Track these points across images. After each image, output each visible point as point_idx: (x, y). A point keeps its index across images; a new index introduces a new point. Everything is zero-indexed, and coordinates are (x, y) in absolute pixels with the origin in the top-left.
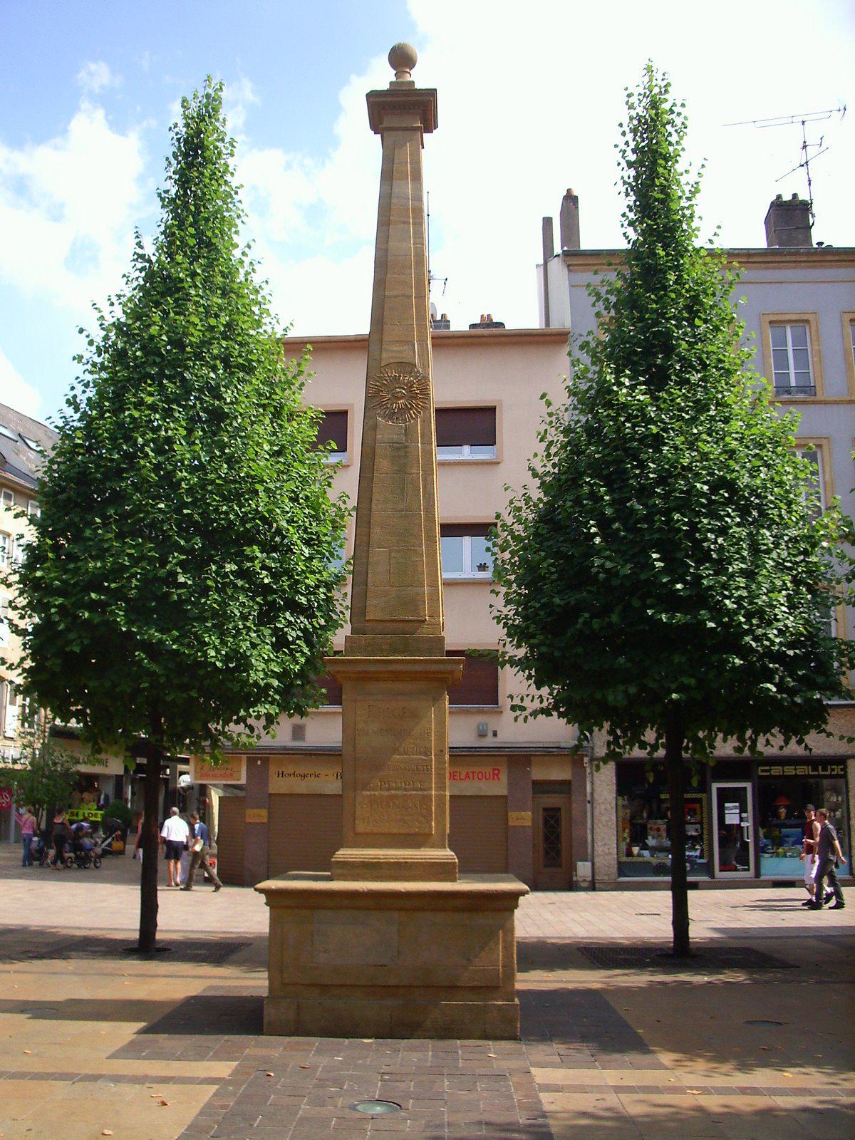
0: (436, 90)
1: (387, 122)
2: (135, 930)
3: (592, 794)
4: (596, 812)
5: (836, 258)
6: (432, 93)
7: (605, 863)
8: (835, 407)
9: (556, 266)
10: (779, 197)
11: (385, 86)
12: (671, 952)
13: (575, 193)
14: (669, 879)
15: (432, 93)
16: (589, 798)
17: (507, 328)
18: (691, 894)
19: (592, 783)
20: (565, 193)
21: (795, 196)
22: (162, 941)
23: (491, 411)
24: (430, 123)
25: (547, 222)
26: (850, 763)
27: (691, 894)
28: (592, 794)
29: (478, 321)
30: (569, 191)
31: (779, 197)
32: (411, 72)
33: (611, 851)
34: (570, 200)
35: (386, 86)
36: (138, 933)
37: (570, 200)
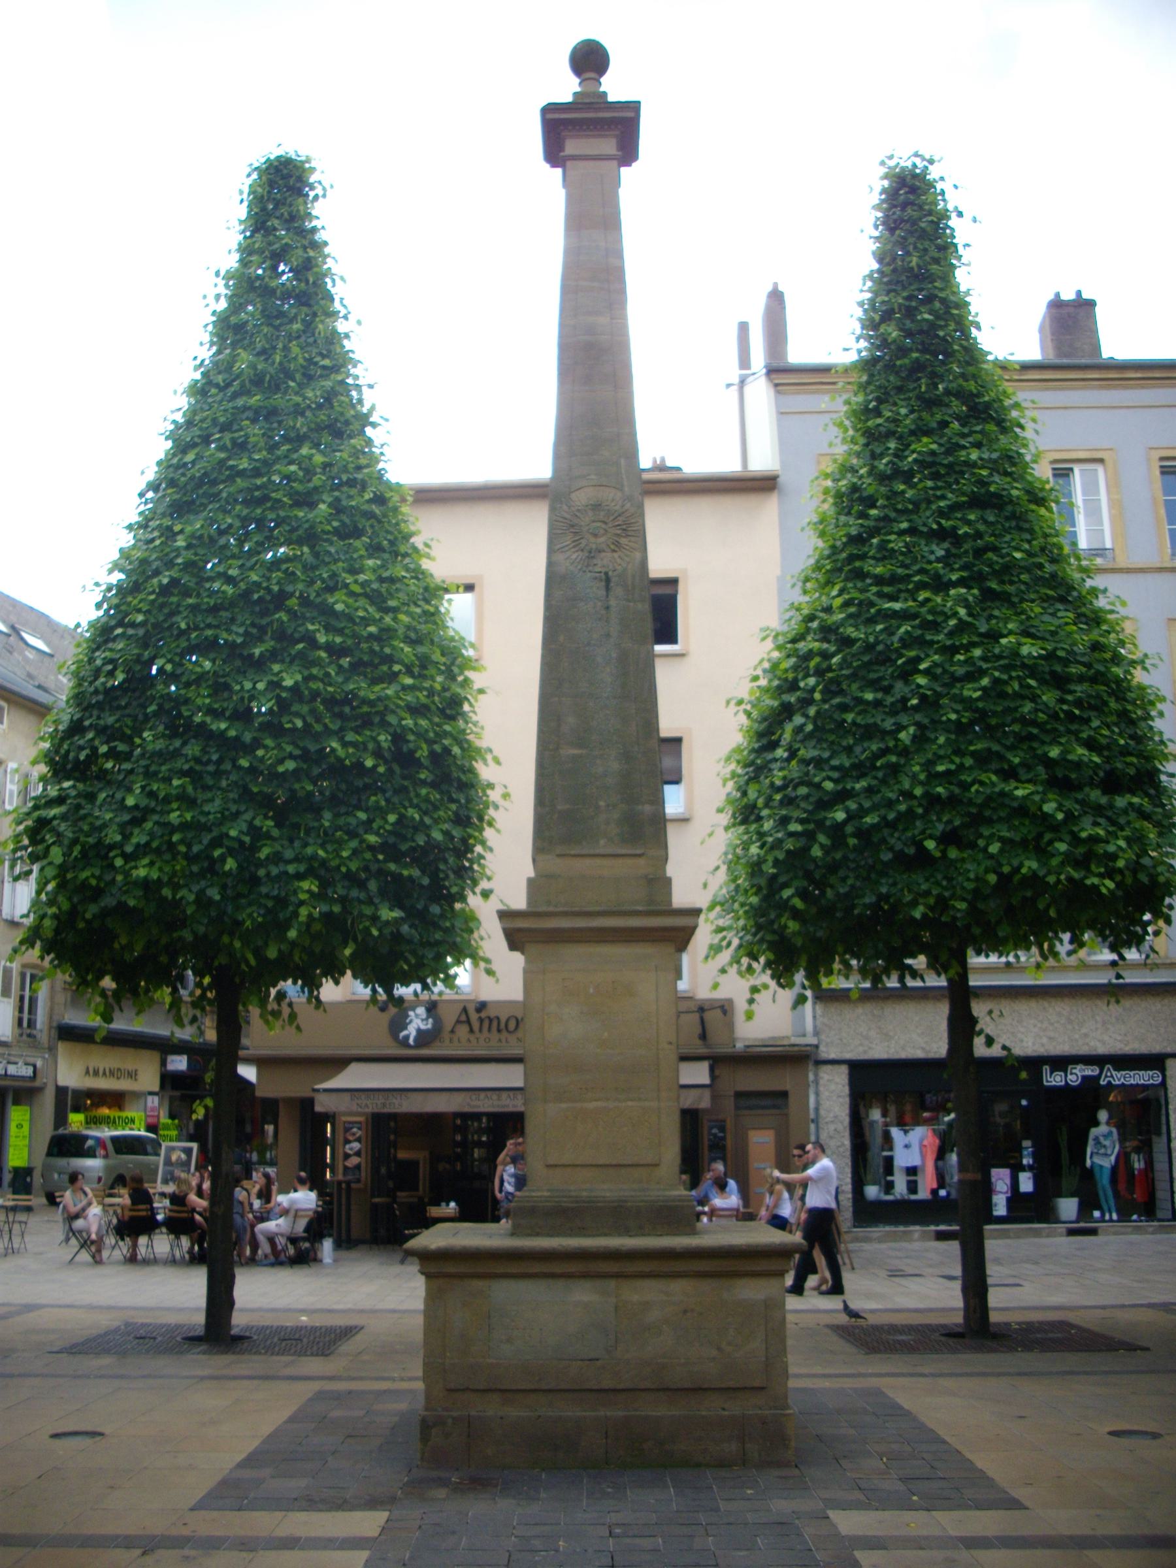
0: (639, 103)
1: (572, 146)
2: (197, 1309)
3: (817, 1109)
5: (1139, 375)
6: (633, 108)
8: (1140, 576)
10: (1057, 295)
12: (960, 1330)
13: (780, 288)
15: (633, 108)
16: (812, 1115)
19: (817, 1094)
21: (1079, 293)
22: (998, 1324)
23: (674, 582)
24: (628, 152)
25: (743, 328)
26: (1170, 1063)
28: (817, 1109)
30: (776, 285)
31: (1057, 295)
34: (776, 298)
35: (568, 98)
36: (961, 1313)
37: (776, 298)
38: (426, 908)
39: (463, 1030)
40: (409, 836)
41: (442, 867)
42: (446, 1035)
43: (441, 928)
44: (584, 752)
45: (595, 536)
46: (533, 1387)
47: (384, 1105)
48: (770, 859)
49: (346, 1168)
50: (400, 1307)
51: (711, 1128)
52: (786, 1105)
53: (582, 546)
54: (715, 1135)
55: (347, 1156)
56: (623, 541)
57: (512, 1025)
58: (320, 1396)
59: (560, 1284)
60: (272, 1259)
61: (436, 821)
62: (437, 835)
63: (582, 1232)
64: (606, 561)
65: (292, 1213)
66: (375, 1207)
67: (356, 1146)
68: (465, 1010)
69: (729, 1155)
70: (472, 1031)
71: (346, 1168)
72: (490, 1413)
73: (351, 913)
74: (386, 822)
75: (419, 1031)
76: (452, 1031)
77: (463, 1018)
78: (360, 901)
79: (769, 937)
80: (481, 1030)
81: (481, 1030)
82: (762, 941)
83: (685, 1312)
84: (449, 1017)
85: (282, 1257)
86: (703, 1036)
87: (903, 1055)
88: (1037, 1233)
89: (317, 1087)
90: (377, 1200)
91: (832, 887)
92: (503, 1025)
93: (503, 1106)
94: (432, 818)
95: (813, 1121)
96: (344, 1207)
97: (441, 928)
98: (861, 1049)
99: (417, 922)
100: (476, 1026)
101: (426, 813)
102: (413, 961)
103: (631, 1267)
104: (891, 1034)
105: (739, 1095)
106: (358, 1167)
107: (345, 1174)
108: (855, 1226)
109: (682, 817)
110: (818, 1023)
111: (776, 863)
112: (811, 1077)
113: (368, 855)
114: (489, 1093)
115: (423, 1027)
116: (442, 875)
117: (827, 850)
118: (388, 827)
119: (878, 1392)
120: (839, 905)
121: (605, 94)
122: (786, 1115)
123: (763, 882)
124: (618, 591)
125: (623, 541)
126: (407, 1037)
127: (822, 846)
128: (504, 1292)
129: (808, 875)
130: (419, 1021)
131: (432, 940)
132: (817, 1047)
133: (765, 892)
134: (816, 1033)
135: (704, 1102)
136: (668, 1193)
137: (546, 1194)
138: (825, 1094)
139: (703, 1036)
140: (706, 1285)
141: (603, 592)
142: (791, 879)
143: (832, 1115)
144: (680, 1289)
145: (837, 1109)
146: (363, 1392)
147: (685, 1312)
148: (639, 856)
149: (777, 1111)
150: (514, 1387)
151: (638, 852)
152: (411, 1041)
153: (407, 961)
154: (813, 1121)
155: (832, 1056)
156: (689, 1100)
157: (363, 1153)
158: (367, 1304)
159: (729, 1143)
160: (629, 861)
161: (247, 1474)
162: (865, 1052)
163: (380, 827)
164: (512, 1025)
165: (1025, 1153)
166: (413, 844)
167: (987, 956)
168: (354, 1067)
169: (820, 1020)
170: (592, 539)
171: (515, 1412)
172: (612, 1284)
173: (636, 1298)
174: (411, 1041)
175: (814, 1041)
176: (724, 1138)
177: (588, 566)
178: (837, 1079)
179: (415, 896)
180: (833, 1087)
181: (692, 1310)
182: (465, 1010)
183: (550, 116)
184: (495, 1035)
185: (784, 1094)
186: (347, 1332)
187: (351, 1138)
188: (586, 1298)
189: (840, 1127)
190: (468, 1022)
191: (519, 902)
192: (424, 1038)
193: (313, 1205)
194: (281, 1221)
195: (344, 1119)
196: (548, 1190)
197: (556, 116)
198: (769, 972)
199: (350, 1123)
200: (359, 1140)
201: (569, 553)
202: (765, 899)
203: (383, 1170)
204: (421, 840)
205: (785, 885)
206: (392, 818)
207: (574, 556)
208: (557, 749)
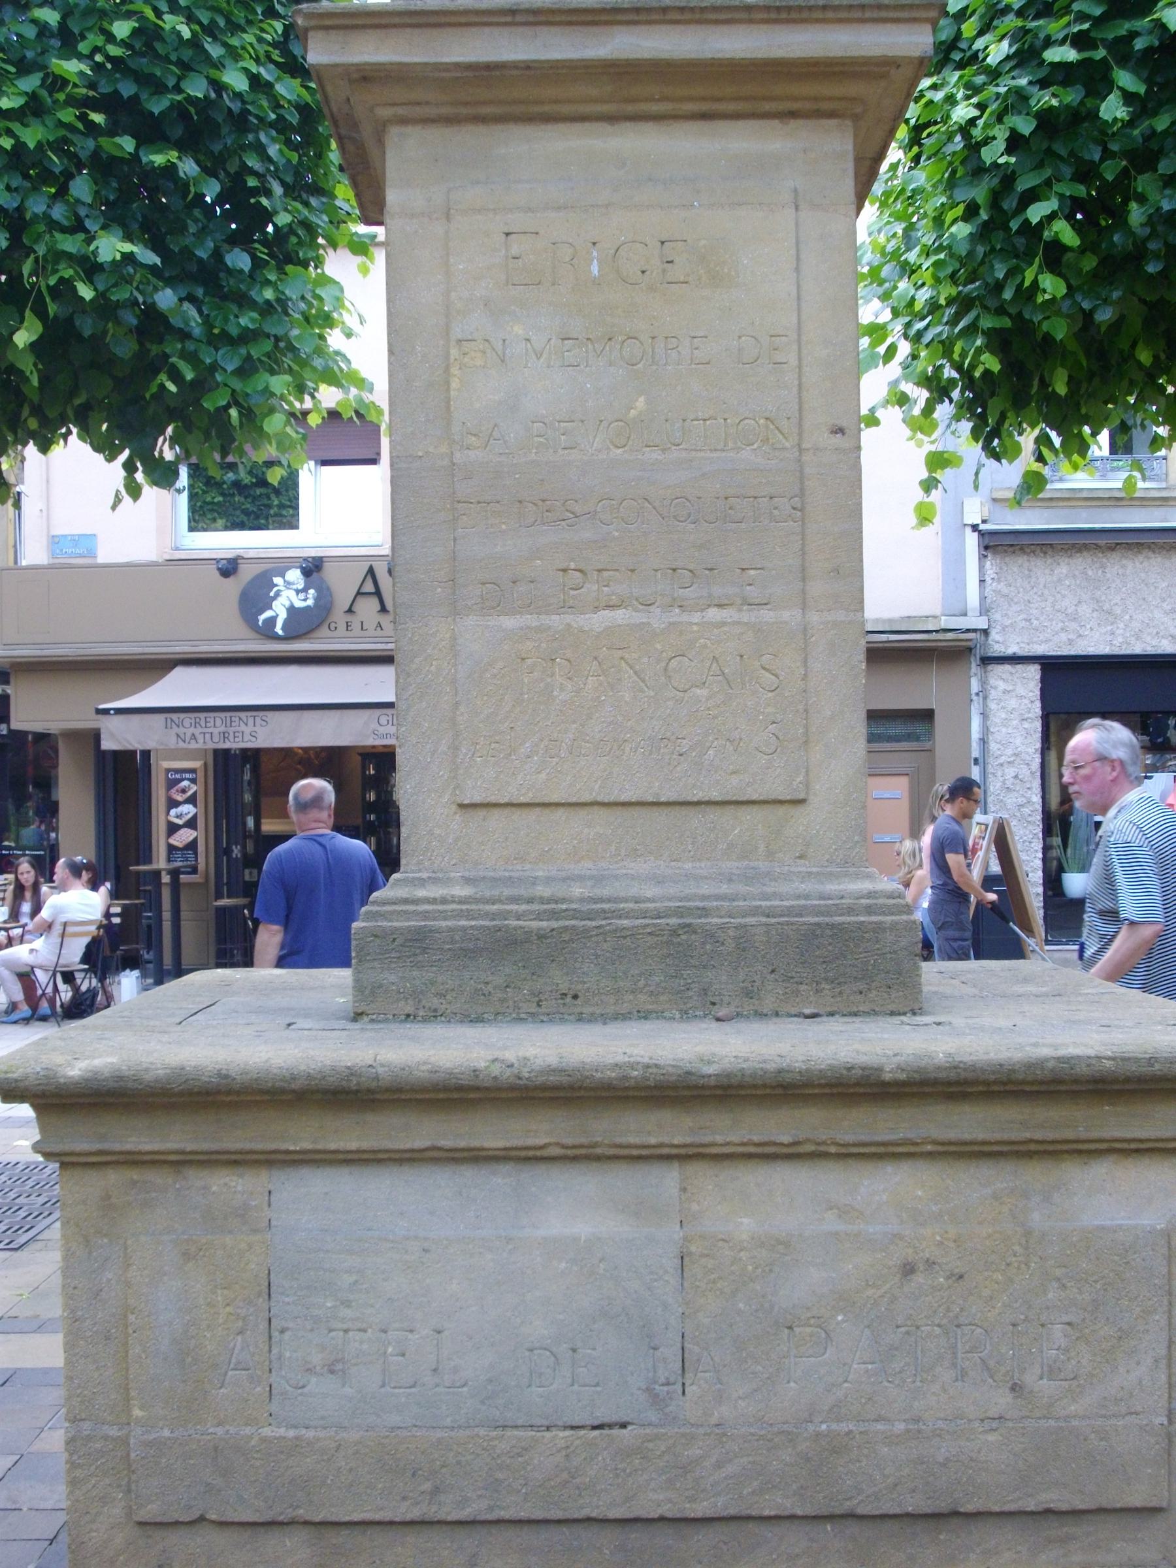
3: (984, 741)
19: (984, 715)
28: (984, 741)
38: (217, 255)
40: (171, 83)
41: (252, 162)
43: (252, 304)
46: (415, 1514)
47: (224, 736)
48: (1001, 134)
49: (171, 849)
52: (930, 734)
55: (173, 829)
59: (501, 1179)
60: (25, 1010)
61: (234, 54)
62: (236, 80)
65: (57, 929)
66: (221, 912)
67: (188, 810)
68: (371, 571)
71: (171, 849)
73: (30, 251)
74: (110, 38)
75: (292, 610)
76: (350, 611)
77: (369, 587)
78: (53, 225)
79: (988, 322)
82: (972, 330)
83: (908, 1270)
84: (344, 587)
85: (44, 1007)
87: (1137, 649)
90: (224, 902)
91: (1142, 199)
94: (225, 45)
97: (252, 304)
98: (1064, 637)
99: (200, 292)
101: (210, 30)
102: (189, 376)
104: (1118, 610)
106: (192, 846)
107: (169, 860)
110: (988, 591)
111: (1015, 142)
112: (975, 686)
113: (68, 115)
115: (299, 604)
116: (252, 182)
117: (1140, 105)
118: (114, 51)
120: (1152, 246)
123: (980, 193)
126: (272, 621)
127: (1129, 97)
129: (1085, 173)
130: (292, 594)
131: (234, 332)
132: (985, 632)
133: (984, 216)
134: (984, 610)
136: (832, 887)
137: (459, 891)
138: (997, 716)
142: (1048, 183)
143: (1009, 752)
145: (1018, 741)
147: (908, 1270)
149: (913, 745)
150: (356, 1517)
152: (279, 630)
153: (176, 376)
154: (976, 761)
155: (1012, 649)
157: (201, 823)
162: (1070, 642)
163: (96, 50)
166: (179, 98)
168: (179, 672)
169: (991, 586)
172: (669, 1179)
173: (746, 1226)
174: (279, 630)
178: (1021, 691)
179: (192, 229)
180: (1013, 703)
181: (930, 1264)
182: (371, 571)
185: (927, 716)
187: (180, 798)
188: (583, 1228)
189: (1024, 772)
190: (378, 593)
193: (97, 914)
194: (39, 943)
195: (166, 764)
196: (468, 881)
198: (966, 426)
199: (177, 771)
200: (192, 800)
202: (983, 233)
203: (236, 851)
204: (197, 88)
205: (1031, 197)
206: (122, 29)
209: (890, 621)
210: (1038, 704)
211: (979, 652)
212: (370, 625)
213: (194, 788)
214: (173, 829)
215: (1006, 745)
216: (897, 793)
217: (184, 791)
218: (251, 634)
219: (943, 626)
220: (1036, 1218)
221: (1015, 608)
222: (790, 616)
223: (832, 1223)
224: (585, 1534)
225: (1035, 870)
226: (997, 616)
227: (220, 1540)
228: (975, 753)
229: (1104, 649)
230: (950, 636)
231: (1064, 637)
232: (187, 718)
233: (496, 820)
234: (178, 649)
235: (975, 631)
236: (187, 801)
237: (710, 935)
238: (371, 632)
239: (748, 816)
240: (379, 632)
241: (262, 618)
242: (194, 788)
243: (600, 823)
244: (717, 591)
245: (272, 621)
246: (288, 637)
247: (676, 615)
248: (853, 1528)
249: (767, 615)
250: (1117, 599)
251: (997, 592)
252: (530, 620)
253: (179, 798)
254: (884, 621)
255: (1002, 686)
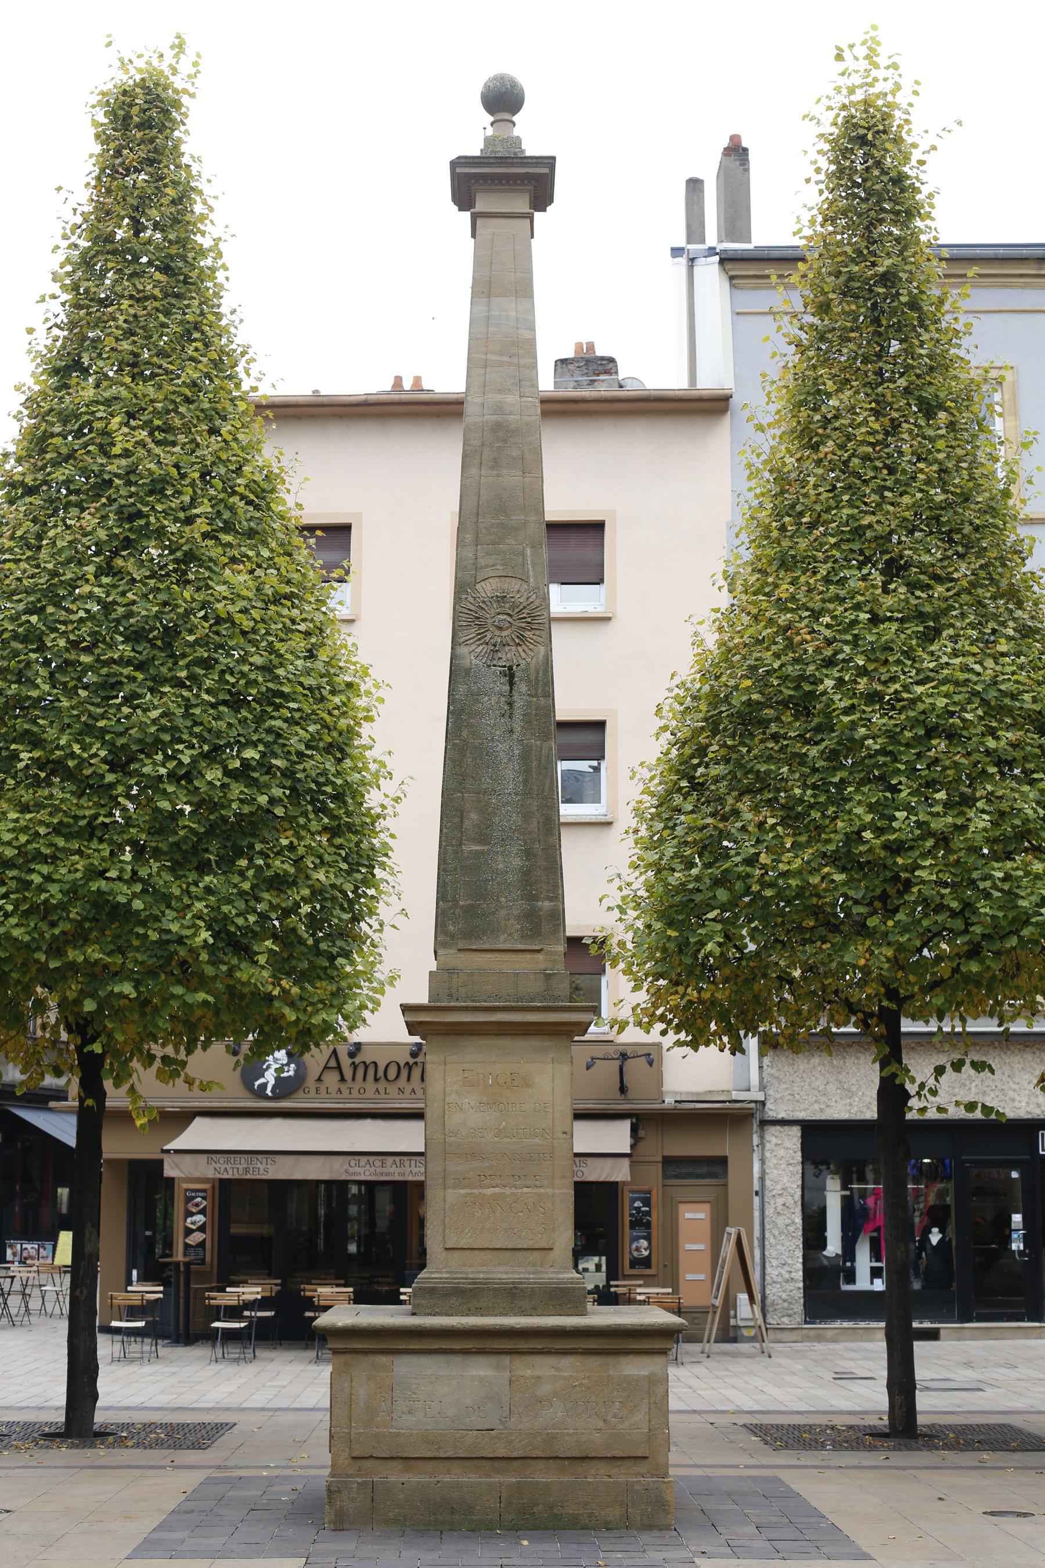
0: (554, 158)
2: (57, 1409)
3: (762, 1179)
4: (769, 1211)
6: (550, 162)
7: (784, 1296)
9: (709, 272)
11: (474, 149)
14: (883, 1325)
15: (550, 162)
17: (623, 373)
18: (920, 1348)
19: (763, 1161)
20: (726, 143)
25: (694, 186)
27: (920, 1348)
28: (762, 1179)
29: (570, 354)
30: (735, 140)
32: (515, 118)
33: (793, 1275)
39: (331, 1079)
42: (311, 1083)
44: (486, 848)
45: (500, 628)
47: (247, 1170)
49: (187, 1246)
50: (269, 1406)
51: (633, 1200)
52: (725, 1173)
53: (487, 639)
54: (638, 1209)
55: (188, 1232)
56: (527, 634)
57: (392, 1073)
58: (208, 1482)
59: (458, 1359)
63: (479, 1311)
64: (509, 655)
67: (200, 1219)
69: (654, 1234)
70: (343, 1079)
71: (187, 1246)
72: (392, 1479)
76: (319, 1080)
77: (333, 1063)
80: (353, 1079)
81: (353, 1079)
86: (623, 1089)
88: (1027, 1333)
89: (165, 1148)
92: (380, 1073)
93: (387, 1174)
95: (757, 1193)
96: (182, 1294)
98: (817, 1106)
100: (348, 1073)
103: (523, 1345)
104: (854, 1089)
105: (668, 1161)
106: (202, 1244)
107: (185, 1255)
108: (806, 1322)
109: (603, 819)
110: (764, 1075)
112: (756, 1140)
114: (371, 1159)
119: (778, 1480)
121: (518, 141)
122: (726, 1185)
124: (522, 687)
125: (527, 634)
126: (264, 1086)
128: (405, 1367)
132: (763, 1103)
134: (762, 1087)
135: (620, 1173)
138: (770, 1164)
139: (623, 1089)
140: (594, 1362)
141: (508, 688)
143: (779, 1187)
144: (568, 1365)
145: (785, 1180)
146: (250, 1478)
148: (539, 951)
151: (537, 948)
152: (269, 1092)
154: (757, 1193)
155: (782, 1115)
156: (596, 1173)
157: (208, 1229)
158: (232, 1402)
159: (654, 1219)
160: (529, 956)
161: (156, 1536)
164: (392, 1073)
165: (1014, 1236)
167: (927, 1022)
168: (198, 1121)
170: (497, 633)
171: (415, 1478)
172: (506, 1360)
173: (528, 1373)
174: (269, 1092)
175: (760, 1097)
176: (648, 1213)
177: (493, 659)
178: (788, 1144)
183: (458, 170)
184: (370, 1085)
185: (723, 1161)
186: (220, 1428)
188: (482, 1373)
189: (790, 1201)
190: (339, 1068)
191: (421, 996)
192: (285, 1087)
195: (185, 1186)
197: (467, 170)
199: (193, 1191)
200: (203, 1212)
201: (473, 647)
207: (479, 650)
208: (460, 845)
209: (697, 1094)
210: (799, 1154)
211: (758, 1116)
212: (333, 1090)
213: (205, 1203)
214: (188, 1232)
215: (776, 1182)
216: (702, 1216)
217: (197, 1205)
218: (247, 1094)
219: (734, 1098)
220: (611, 1372)
221: (783, 1086)
222: (549, 1191)
223: (553, 1372)
224: (482, 1462)
225: (797, 1271)
226: (771, 1092)
227: (377, 1463)
228: (756, 1187)
229: (845, 1116)
230: (737, 1105)
231: (817, 1106)
232: (222, 1158)
233: (457, 1253)
234: (197, 1104)
235: (755, 1102)
236: (199, 1213)
237: (522, 1290)
238: (333, 1095)
239: (535, 1253)
240: (339, 1096)
241: (257, 1083)
242: (205, 1203)
243: (487, 1256)
244: (528, 1183)
245: (264, 1086)
246: (275, 1098)
247: (513, 1190)
248: (558, 1461)
249: (542, 1190)
250: (854, 1081)
251: (771, 1075)
252: (468, 1191)
253: (194, 1210)
254: (693, 1094)
255: (774, 1140)
